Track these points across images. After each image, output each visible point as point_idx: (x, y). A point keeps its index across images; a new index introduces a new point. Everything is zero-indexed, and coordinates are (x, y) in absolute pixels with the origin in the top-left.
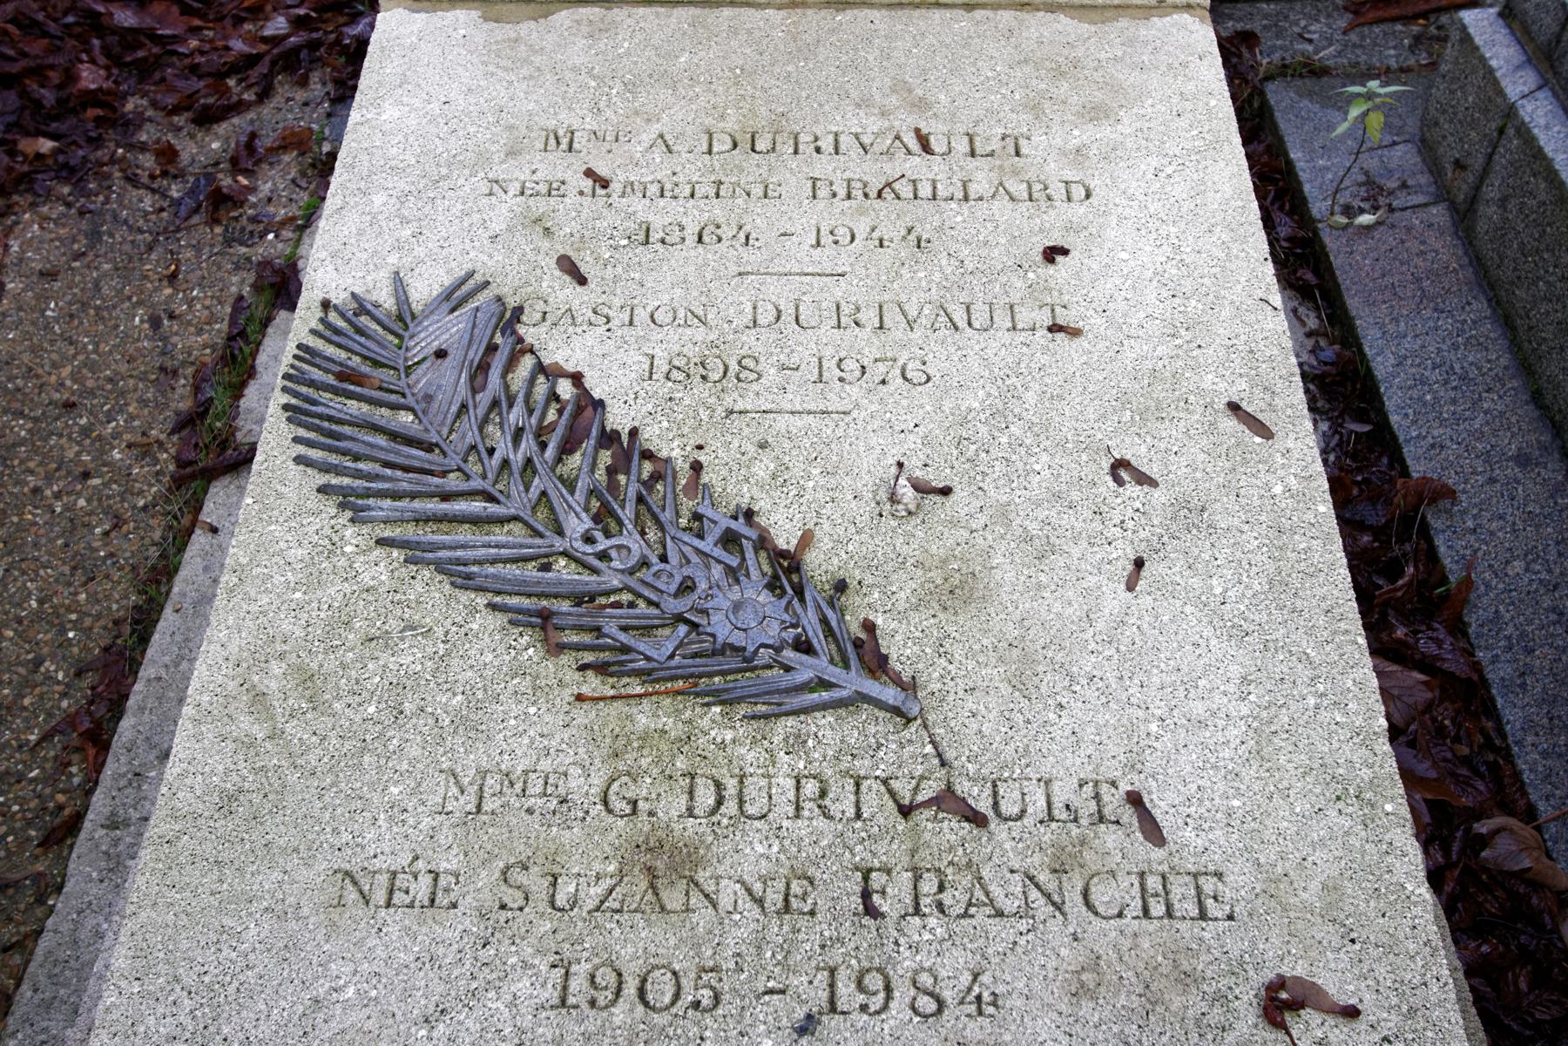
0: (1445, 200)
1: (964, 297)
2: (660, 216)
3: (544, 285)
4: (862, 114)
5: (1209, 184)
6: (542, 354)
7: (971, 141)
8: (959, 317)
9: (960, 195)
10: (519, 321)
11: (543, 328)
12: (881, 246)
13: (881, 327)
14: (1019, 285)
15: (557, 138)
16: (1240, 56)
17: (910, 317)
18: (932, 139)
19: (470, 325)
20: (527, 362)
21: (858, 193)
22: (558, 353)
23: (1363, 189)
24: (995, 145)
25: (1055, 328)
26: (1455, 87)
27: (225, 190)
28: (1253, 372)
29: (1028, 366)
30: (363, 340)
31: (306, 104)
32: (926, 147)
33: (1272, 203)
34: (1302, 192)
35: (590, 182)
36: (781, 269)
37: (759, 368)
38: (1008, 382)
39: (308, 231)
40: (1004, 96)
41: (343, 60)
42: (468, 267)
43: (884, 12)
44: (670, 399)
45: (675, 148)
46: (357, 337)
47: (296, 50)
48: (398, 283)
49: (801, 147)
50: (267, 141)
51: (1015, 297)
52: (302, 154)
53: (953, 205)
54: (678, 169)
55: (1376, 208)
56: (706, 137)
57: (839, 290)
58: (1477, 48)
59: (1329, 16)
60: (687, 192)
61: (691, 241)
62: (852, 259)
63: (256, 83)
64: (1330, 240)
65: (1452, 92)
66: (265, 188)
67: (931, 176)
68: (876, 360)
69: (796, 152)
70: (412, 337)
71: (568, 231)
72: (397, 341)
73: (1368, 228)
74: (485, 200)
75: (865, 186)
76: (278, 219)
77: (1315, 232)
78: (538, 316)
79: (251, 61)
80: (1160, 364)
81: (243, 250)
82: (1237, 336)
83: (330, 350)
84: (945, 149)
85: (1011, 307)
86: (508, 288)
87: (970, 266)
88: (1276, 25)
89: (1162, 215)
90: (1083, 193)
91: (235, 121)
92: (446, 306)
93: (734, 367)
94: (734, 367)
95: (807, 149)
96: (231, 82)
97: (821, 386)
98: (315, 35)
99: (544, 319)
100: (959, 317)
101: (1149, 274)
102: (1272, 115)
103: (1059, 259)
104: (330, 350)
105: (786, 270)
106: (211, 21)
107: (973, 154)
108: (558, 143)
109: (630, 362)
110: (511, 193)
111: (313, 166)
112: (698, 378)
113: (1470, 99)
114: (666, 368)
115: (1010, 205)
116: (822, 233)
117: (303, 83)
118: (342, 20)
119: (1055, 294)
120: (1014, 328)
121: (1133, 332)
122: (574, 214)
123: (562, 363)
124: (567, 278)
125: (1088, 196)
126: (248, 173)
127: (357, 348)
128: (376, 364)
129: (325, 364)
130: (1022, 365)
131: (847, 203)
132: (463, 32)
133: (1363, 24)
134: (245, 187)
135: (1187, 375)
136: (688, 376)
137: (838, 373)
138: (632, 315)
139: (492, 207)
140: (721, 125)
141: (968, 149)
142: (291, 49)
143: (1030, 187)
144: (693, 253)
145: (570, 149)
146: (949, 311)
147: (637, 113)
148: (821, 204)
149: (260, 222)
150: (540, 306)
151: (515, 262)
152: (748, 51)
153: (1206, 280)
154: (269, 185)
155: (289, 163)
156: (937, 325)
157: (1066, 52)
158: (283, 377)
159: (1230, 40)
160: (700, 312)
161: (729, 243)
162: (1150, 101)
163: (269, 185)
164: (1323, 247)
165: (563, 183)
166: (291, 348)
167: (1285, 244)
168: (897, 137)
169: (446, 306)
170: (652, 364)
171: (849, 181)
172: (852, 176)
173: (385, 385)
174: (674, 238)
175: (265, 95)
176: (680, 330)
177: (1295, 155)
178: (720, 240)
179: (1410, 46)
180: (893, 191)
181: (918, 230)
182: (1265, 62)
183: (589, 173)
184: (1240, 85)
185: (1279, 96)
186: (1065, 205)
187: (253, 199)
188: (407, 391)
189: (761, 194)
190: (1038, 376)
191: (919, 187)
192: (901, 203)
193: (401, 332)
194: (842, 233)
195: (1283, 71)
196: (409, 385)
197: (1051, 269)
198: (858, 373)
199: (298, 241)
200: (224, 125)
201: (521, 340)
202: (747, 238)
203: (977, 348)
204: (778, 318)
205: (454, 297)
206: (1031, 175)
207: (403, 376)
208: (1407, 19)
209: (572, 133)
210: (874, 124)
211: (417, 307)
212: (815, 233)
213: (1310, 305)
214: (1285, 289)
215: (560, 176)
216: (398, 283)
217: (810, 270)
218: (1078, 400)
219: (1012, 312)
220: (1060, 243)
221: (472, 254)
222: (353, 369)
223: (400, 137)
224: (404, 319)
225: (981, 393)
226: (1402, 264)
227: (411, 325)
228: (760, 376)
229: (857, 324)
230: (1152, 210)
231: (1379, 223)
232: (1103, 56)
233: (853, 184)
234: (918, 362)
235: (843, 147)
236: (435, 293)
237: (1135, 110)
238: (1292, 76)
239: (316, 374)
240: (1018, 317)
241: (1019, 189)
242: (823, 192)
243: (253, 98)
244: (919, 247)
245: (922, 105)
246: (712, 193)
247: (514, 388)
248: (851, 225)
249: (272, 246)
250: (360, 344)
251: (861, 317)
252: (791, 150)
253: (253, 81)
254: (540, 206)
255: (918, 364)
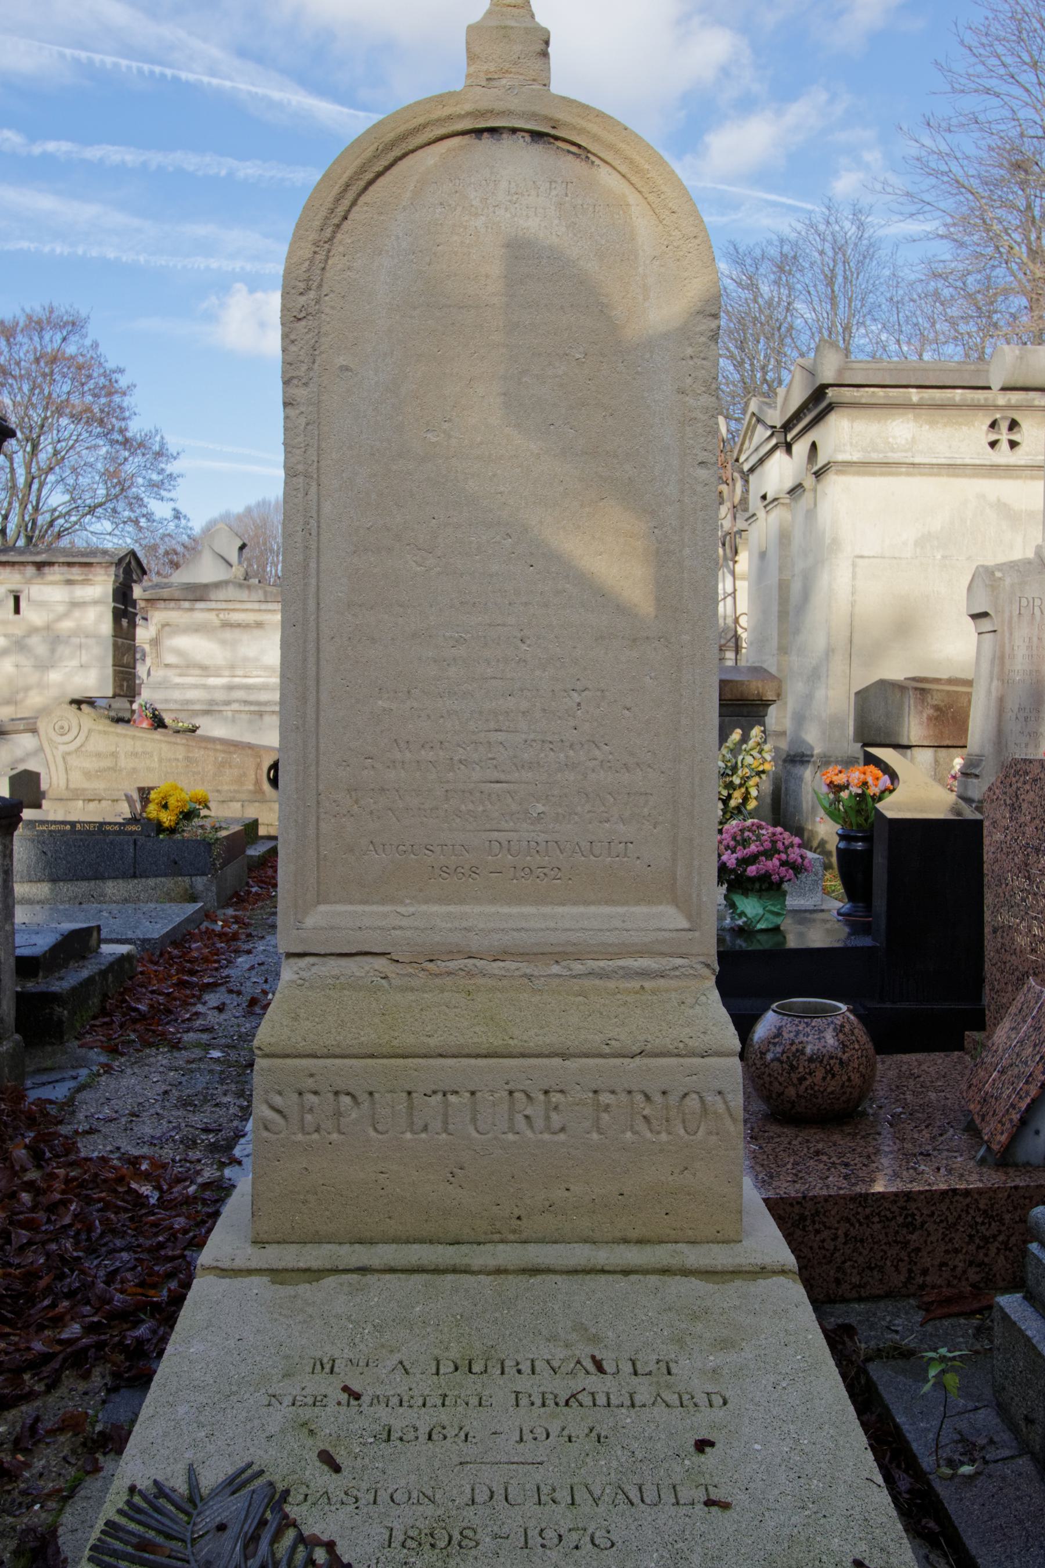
0: (1027, 1453)
1: (637, 1479)
2: (399, 1420)
3: (307, 1473)
4: (551, 1346)
5: (815, 1394)
6: (303, 1527)
7: (634, 1364)
8: (634, 1495)
9: (629, 1403)
10: (285, 1502)
11: (305, 1507)
12: (570, 1441)
13: (573, 1504)
14: (678, 1470)
15: (322, 1365)
16: (844, 1343)
17: (595, 1496)
18: (604, 1363)
19: (247, 1504)
20: (291, 1534)
21: (550, 1402)
22: (315, 1525)
23: (960, 1445)
24: (652, 1366)
25: (709, 1503)
26: (1008, 1356)
27: (6, 1465)
28: (870, 1536)
29: (691, 1534)
30: (159, 1517)
31: (86, 1393)
32: (600, 1369)
33: (890, 1462)
34: (911, 1450)
35: (346, 1396)
36: (493, 1460)
37: (477, 1537)
38: (677, 1546)
39: (71, 1501)
40: (656, 1333)
41: (122, 1357)
42: (247, 1459)
43: (564, 1276)
44: (405, 1563)
45: (411, 1371)
46: (156, 1515)
47: (86, 1349)
48: (191, 1473)
49: (506, 1370)
50: (49, 1422)
51: (677, 1479)
52: (76, 1435)
53: (624, 1410)
54: (414, 1386)
55: (972, 1462)
56: (435, 1363)
57: (538, 1476)
58: (1014, 1323)
59: (907, 1313)
60: (420, 1402)
61: (423, 1437)
62: (548, 1451)
63: (48, 1377)
64: (943, 1491)
65: (1008, 1360)
66: (39, 1464)
67: (605, 1389)
68: (570, 1530)
69: (503, 1373)
70: (199, 1514)
71: (328, 1431)
72: (186, 1518)
73: (970, 1478)
74: (265, 1409)
75: (556, 1397)
76: (46, 1491)
77: (928, 1483)
78: (301, 1497)
79: (46, 1358)
80: (796, 1530)
81: (10, 1520)
82: (853, 1508)
83: (132, 1526)
84: (614, 1370)
85: (674, 1487)
86: (278, 1475)
87: (639, 1455)
88: (868, 1320)
89: (782, 1416)
90: (721, 1401)
91: (24, 1408)
92: (228, 1490)
93: (457, 1536)
94: (457, 1536)
95: (511, 1370)
96: (27, 1377)
97: (527, 1551)
98: (103, 1337)
99: (305, 1500)
100: (634, 1495)
101: (779, 1460)
102: (877, 1389)
103: (708, 1449)
104: (132, 1526)
105: (497, 1460)
106: (18, 1329)
107: (636, 1373)
108: (323, 1368)
109: (373, 1533)
110: (285, 1404)
111: (84, 1444)
112: (428, 1546)
113: (1021, 1364)
114: (402, 1538)
115: (667, 1410)
116: (524, 1432)
117: (86, 1376)
118: (125, 1326)
119: (707, 1476)
120: (678, 1504)
121: (771, 1506)
122: (333, 1419)
123: (319, 1534)
124: (326, 1468)
125: (725, 1403)
126: (26, 1451)
127: (154, 1523)
128: (169, 1537)
129: (126, 1537)
130: (687, 1533)
131: (542, 1410)
132: (256, 1291)
133: (934, 1319)
134: (22, 1462)
135: (818, 1539)
136: (420, 1544)
137: (540, 1540)
138: (375, 1496)
139: (269, 1415)
140: (446, 1354)
141: (631, 1370)
142: (82, 1348)
143: (680, 1398)
144: (424, 1447)
145: (332, 1372)
146: (625, 1490)
147: (383, 1346)
148: (522, 1411)
149: (29, 1494)
150: (303, 1490)
151: (285, 1455)
152: (466, 1303)
153: (822, 1465)
154: (42, 1462)
155: (63, 1443)
156: (617, 1502)
157: (698, 1302)
158: (91, 1549)
159: (834, 1331)
160: (430, 1493)
161: (452, 1440)
162: (763, 1336)
163: (42, 1462)
164: (937, 1496)
165: (325, 1396)
166: (100, 1525)
167: (907, 1496)
168: (578, 1362)
169: (228, 1490)
170: (391, 1535)
171: (543, 1394)
172: (545, 1390)
173: (174, 1554)
174: (411, 1435)
175: (50, 1388)
176: (414, 1507)
177: (900, 1419)
178: (445, 1438)
179: (974, 1335)
180: (577, 1400)
181: (598, 1428)
182: (863, 1346)
183: (346, 1389)
184: (847, 1365)
185: (878, 1372)
186: (709, 1409)
187: (27, 1474)
188: (191, 1558)
189: (477, 1403)
190: (700, 1541)
191: (597, 1397)
192: (583, 1409)
193: (191, 1510)
194: (540, 1432)
195: (878, 1354)
196: (193, 1553)
197: (702, 1458)
198: (556, 1541)
199: (61, 1511)
200: (14, 1412)
201: (286, 1516)
202: (466, 1436)
203: (649, 1519)
204: (491, 1498)
205: (235, 1483)
206: (681, 1388)
207: (189, 1546)
208: (969, 1314)
209: (334, 1361)
210: (560, 1353)
211: (205, 1492)
212: (518, 1432)
213: (939, 1552)
214: (914, 1538)
215: (323, 1391)
216: (191, 1473)
217: (516, 1459)
218: (733, 1560)
219: (675, 1491)
220: (707, 1437)
221: (252, 1450)
222: (149, 1540)
223: (203, 1364)
224: (194, 1500)
225: (655, 1555)
226: (1005, 1508)
227: (199, 1505)
228: (478, 1544)
229: (554, 1501)
230: (775, 1413)
231: (978, 1474)
232: (725, 1305)
233: (547, 1396)
234: (604, 1531)
235: (538, 1369)
236: (220, 1480)
237: (753, 1342)
238: (887, 1358)
239: (118, 1545)
240: (679, 1494)
241: (673, 1399)
242: (524, 1401)
243: (43, 1388)
244: (599, 1442)
245: (595, 1339)
246: (439, 1402)
247: (278, 1556)
248: (546, 1426)
249: (37, 1515)
250: (157, 1520)
251: (557, 1495)
252: (499, 1372)
253: (45, 1375)
254: (307, 1413)
255: (604, 1533)
